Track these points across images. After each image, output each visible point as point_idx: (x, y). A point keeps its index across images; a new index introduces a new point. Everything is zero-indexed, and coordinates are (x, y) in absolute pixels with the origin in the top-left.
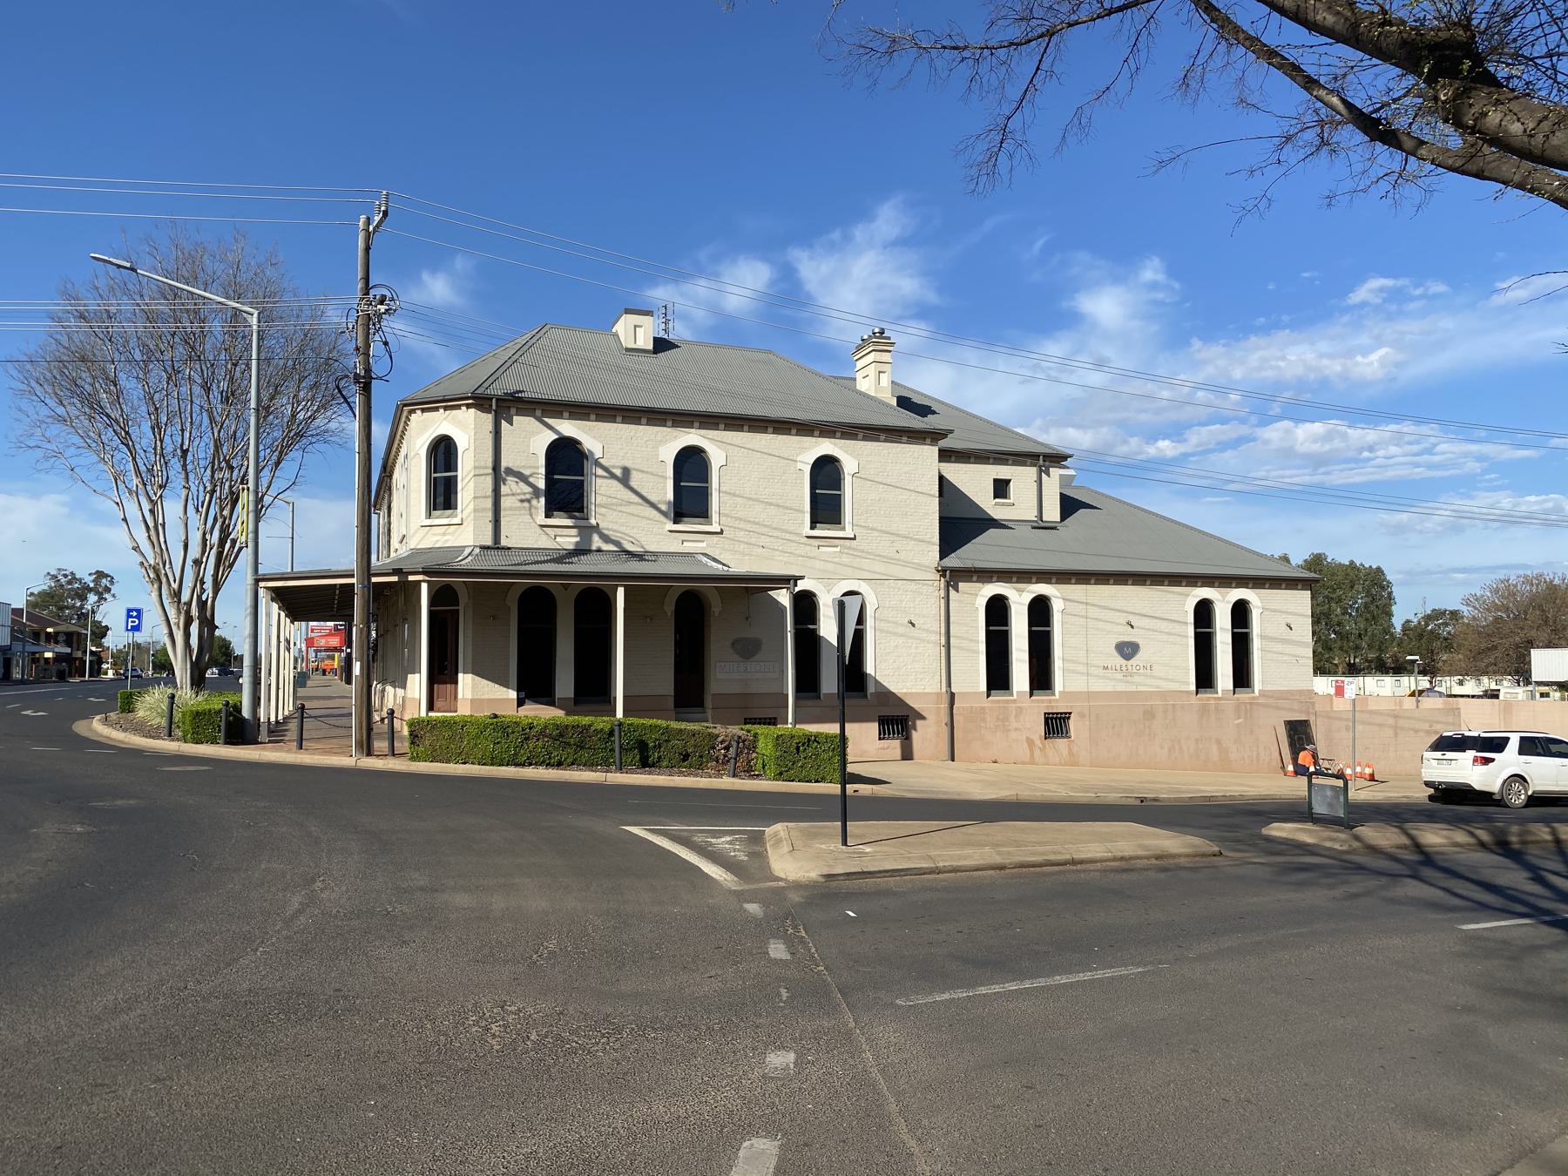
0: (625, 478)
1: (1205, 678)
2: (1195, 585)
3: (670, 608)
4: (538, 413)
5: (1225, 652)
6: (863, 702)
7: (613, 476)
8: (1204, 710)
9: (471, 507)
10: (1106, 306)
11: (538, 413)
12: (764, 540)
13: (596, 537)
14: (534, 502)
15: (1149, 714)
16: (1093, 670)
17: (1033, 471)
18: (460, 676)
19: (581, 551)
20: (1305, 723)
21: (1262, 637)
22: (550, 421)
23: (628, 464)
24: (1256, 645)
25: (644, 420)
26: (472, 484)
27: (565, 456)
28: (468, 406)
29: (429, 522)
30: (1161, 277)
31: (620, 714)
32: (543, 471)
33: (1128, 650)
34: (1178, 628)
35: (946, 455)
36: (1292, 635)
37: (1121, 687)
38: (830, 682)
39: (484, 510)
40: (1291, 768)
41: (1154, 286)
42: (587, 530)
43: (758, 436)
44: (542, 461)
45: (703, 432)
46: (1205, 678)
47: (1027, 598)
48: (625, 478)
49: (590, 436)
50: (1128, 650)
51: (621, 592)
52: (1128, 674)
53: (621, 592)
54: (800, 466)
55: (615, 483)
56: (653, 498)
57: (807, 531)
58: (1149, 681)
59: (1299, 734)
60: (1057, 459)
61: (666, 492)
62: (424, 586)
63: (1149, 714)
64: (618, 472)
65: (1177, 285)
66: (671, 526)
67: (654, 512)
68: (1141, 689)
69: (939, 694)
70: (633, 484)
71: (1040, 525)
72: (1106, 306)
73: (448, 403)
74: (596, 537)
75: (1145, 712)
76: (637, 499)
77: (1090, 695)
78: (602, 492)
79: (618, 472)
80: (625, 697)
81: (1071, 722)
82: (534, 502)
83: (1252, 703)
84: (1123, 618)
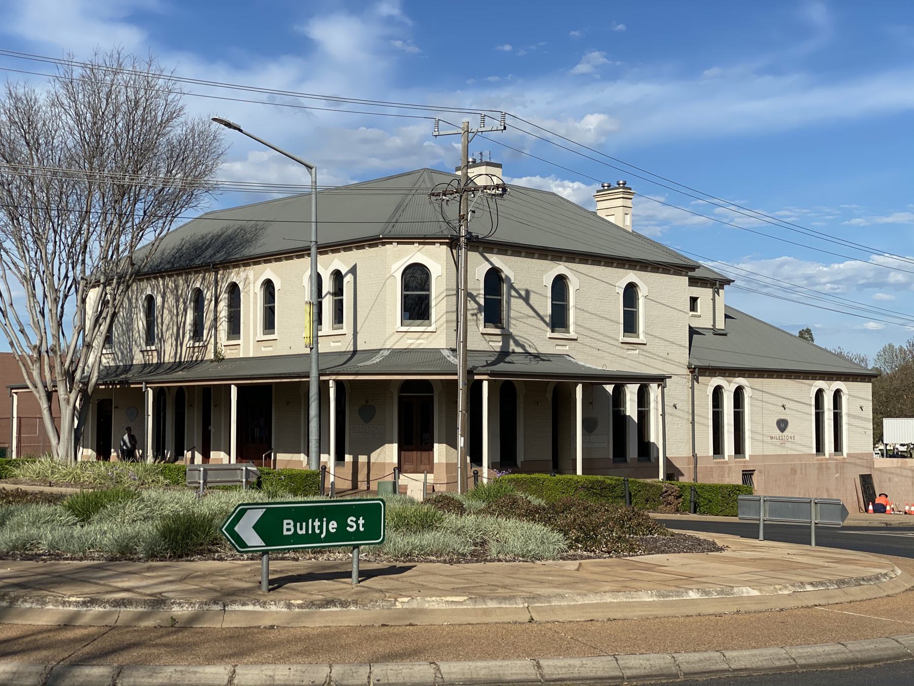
0: (526, 299)
1: (820, 448)
2: (814, 379)
3: (549, 396)
4: (481, 249)
5: (827, 422)
6: (623, 465)
7: (520, 296)
8: (820, 467)
9: (444, 319)
10: (338, 36)
11: (481, 249)
12: (599, 345)
13: (511, 342)
14: (479, 316)
15: (794, 471)
16: (765, 439)
17: (710, 291)
18: (436, 445)
19: (504, 354)
20: (869, 476)
21: (849, 415)
22: (486, 255)
23: (529, 288)
24: (845, 420)
25: (603, 263)
26: (444, 302)
27: (494, 278)
28: (441, 244)
29: (405, 329)
30: (396, 12)
31: (579, 471)
32: (482, 292)
33: (782, 425)
34: (805, 408)
35: (694, 282)
36: (862, 414)
37: (780, 451)
38: (632, 451)
39: (452, 321)
40: (871, 507)
41: (389, 21)
42: (507, 336)
43: (596, 268)
44: (482, 286)
45: (567, 264)
46: (820, 448)
47: (733, 387)
48: (526, 299)
49: (506, 265)
50: (782, 425)
51: (579, 389)
52: (783, 442)
53: (579, 389)
54: (617, 290)
55: (521, 301)
56: (541, 313)
57: (621, 338)
58: (794, 446)
59: (866, 481)
60: (717, 283)
61: (546, 309)
62: (485, 385)
63: (794, 471)
64: (523, 293)
65: (410, 22)
66: (549, 334)
67: (542, 323)
68: (790, 452)
69: (689, 458)
70: (531, 302)
71: (717, 333)
72: (338, 36)
73: (425, 240)
74: (511, 342)
75: (792, 469)
76: (533, 314)
77: (765, 457)
78: (516, 308)
79: (523, 293)
80: (583, 459)
81: (753, 477)
82: (479, 316)
83: (844, 461)
84: (781, 402)
